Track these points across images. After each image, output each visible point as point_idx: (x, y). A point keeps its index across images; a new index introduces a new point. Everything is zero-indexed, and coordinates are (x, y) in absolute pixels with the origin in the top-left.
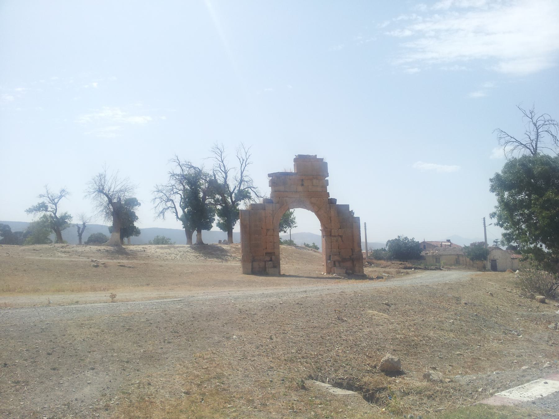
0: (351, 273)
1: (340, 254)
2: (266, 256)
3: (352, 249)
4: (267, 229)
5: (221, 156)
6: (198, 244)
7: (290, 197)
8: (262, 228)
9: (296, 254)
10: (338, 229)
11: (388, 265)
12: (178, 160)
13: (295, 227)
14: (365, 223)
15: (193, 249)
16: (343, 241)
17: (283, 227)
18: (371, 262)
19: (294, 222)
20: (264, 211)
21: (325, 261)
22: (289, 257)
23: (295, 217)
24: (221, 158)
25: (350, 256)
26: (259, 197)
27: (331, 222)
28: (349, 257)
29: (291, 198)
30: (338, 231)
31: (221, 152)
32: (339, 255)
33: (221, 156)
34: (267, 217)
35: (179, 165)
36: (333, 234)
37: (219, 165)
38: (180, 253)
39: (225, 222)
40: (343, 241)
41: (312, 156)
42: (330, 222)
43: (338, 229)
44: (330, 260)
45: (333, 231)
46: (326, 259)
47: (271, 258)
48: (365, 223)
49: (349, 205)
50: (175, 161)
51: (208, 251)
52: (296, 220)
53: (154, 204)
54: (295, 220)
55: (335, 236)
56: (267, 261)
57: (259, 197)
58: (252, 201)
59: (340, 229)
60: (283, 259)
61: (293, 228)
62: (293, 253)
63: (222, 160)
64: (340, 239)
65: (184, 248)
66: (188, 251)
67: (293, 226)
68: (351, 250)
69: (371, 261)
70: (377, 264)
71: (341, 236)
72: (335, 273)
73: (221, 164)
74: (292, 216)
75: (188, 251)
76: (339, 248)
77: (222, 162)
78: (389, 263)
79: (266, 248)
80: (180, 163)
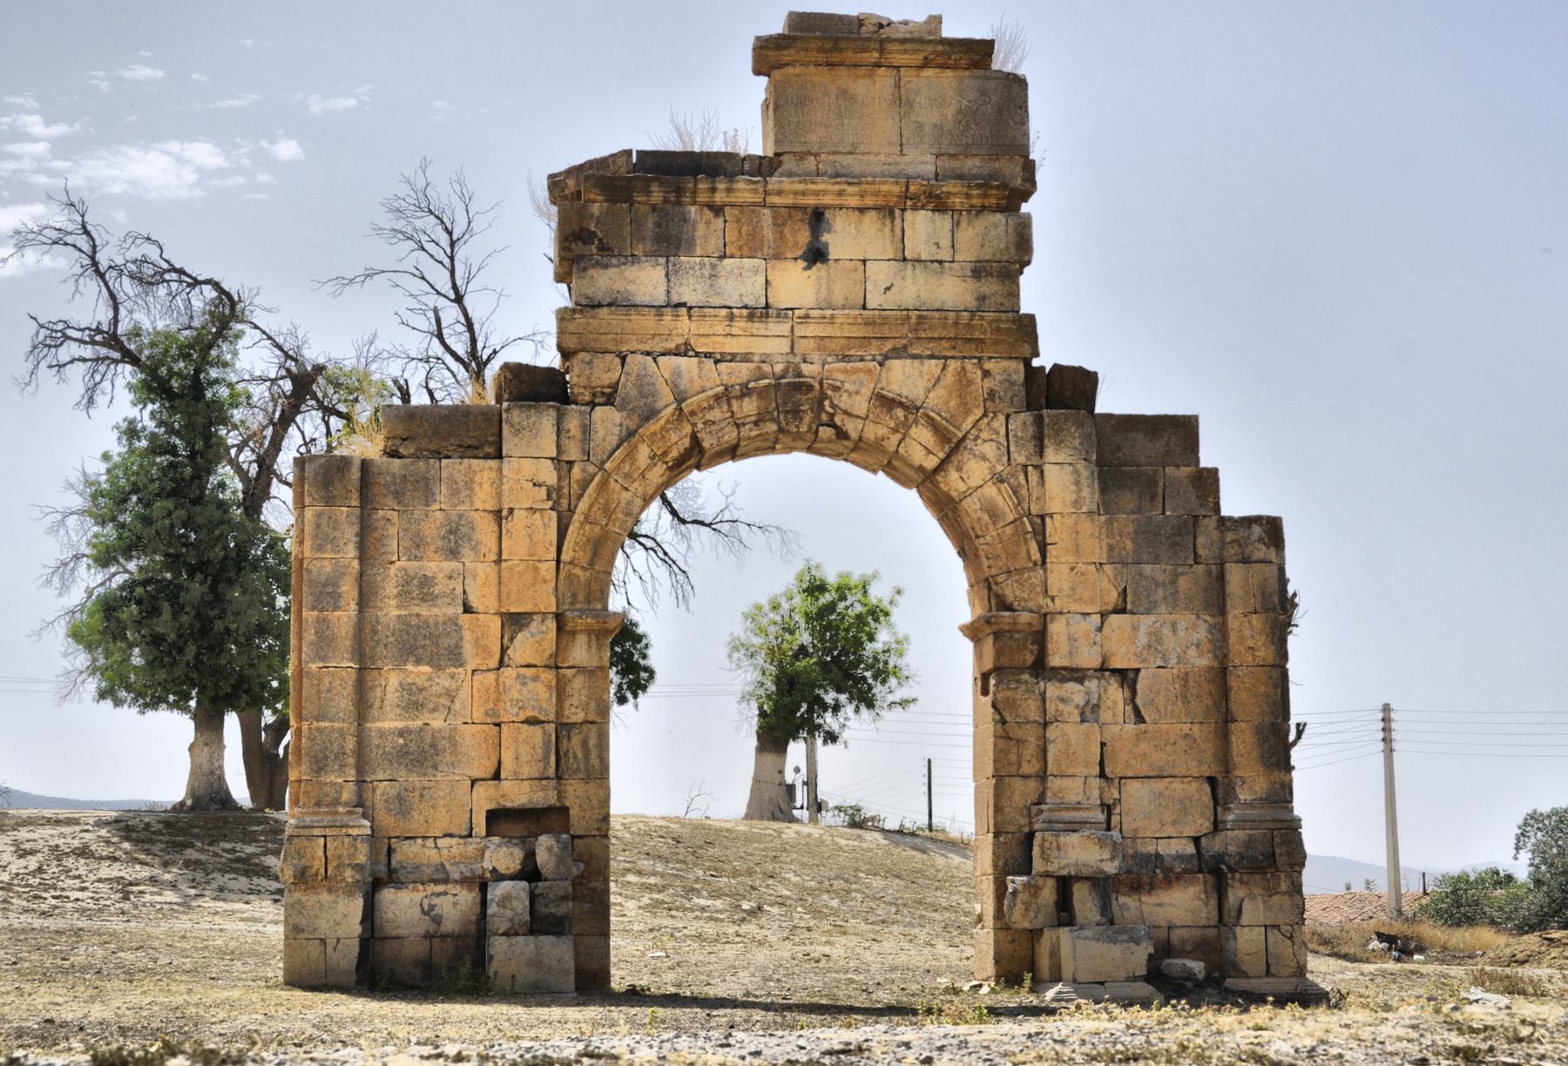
0: (1201, 976)
1: (1115, 819)
2: (496, 839)
3: (1212, 781)
4: (511, 615)
5: (447, 261)
6: (192, 808)
7: (708, 355)
8: (468, 609)
9: (877, 883)
10: (1104, 615)
11: (1520, 956)
12: (87, 232)
13: (904, 703)
14: (1386, 708)
15: (128, 839)
16: (1140, 718)
17: (819, 705)
18: (1407, 939)
19: (896, 672)
20: (493, 463)
21: (988, 886)
22: (825, 897)
23: (907, 639)
24: (452, 272)
25: (1196, 841)
26: (683, 521)
27: (1044, 556)
28: (1191, 849)
29: (717, 362)
30: (1100, 629)
31: (450, 233)
32: (457, 381)
33: (452, 258)
34: (511, 510)
35: (95, 264)
36: (1055, 660)
37: (431, 314)
38: (23, 862)
39: (167, 566)
40: (1140, 718)
41: (906, 23)
42: (1036, 556)
43: (1104, 615)
44: (1028, 873)
45: (1057, 629)
46: (995, 866)
47: (530, 856)
48: (1386, 708)
49: (1196, 418)
50: (69, 239)
51: (233, 851)
52: (910, 661)
53: (60, 595)
54: (901, 662)
55: (1076, 675)
56: (499, 877)
57: (683, 521)
58: (646, 549)
59: (1114, 619)
60: (775, 910)
61: (884, 713)
62: (857, 870)
63: (455, 287)
64: (1115, 693)
65: (67, 830)
66: (86, 846)
67: (891, 698)
68: (1207, 788)
69: (1409, 932)
70: (1445, 948)
71: (1128, 678)
72: (1058, 980)
73: (451, 314)
74: (883, 637)
75: (86, 846)
76: (1102, 775)
77: (459, 299)
78: (1531, 941)
79: (497, 776)
80: (98, 256)
